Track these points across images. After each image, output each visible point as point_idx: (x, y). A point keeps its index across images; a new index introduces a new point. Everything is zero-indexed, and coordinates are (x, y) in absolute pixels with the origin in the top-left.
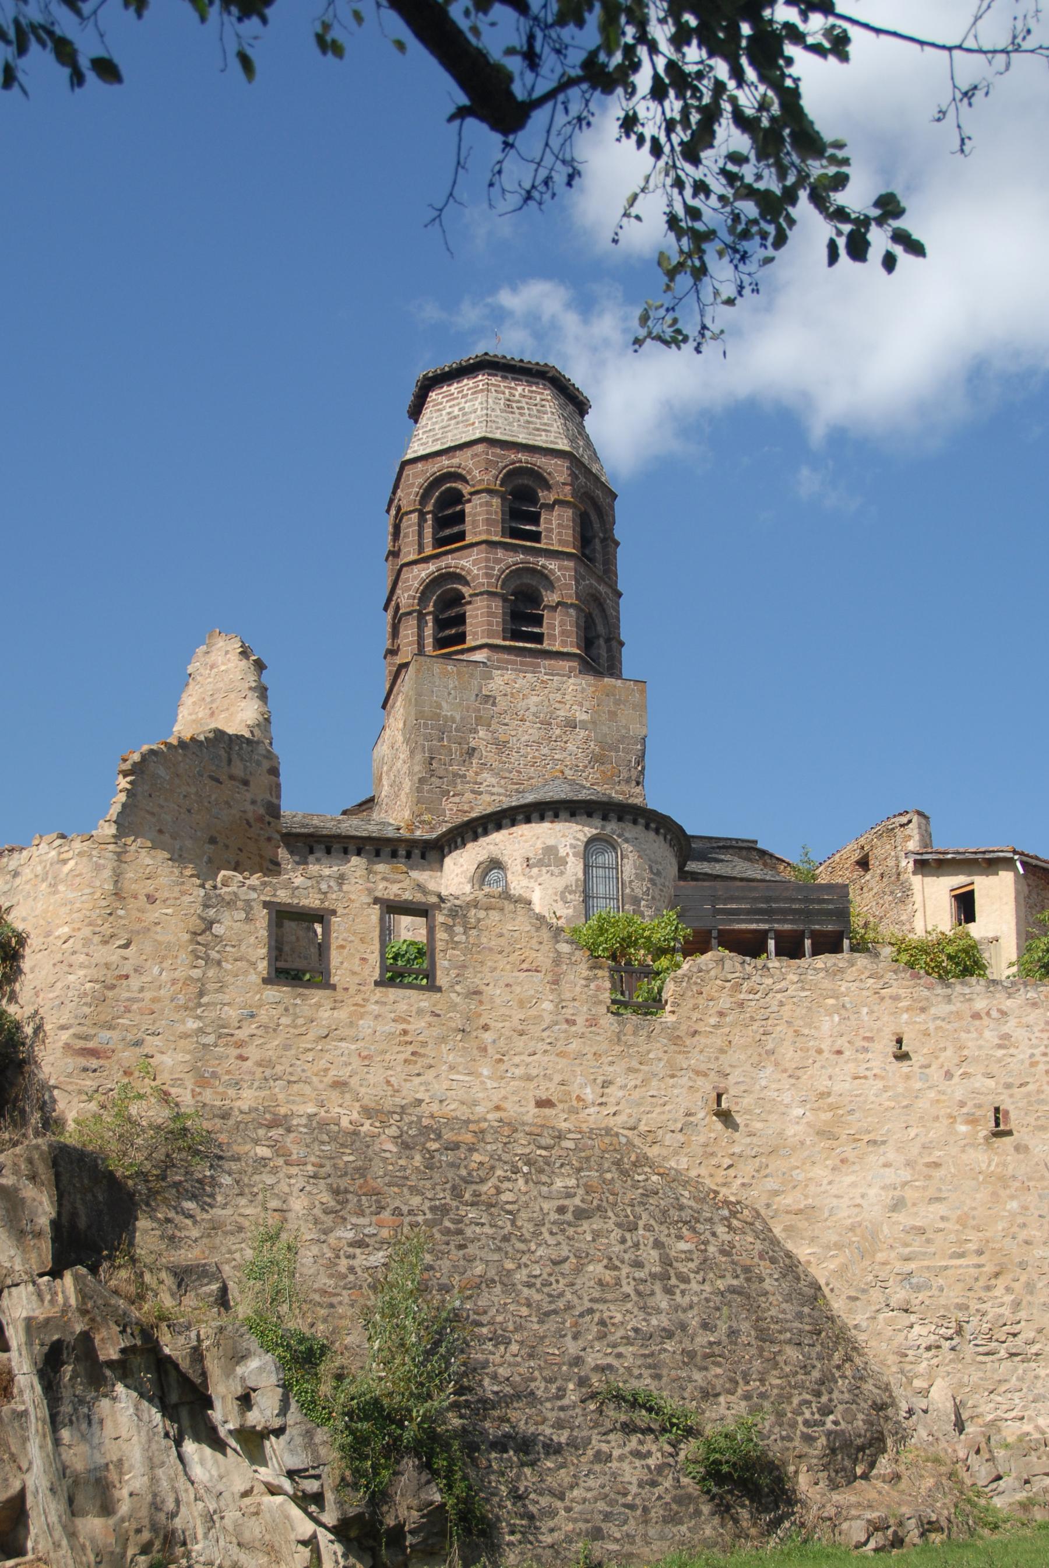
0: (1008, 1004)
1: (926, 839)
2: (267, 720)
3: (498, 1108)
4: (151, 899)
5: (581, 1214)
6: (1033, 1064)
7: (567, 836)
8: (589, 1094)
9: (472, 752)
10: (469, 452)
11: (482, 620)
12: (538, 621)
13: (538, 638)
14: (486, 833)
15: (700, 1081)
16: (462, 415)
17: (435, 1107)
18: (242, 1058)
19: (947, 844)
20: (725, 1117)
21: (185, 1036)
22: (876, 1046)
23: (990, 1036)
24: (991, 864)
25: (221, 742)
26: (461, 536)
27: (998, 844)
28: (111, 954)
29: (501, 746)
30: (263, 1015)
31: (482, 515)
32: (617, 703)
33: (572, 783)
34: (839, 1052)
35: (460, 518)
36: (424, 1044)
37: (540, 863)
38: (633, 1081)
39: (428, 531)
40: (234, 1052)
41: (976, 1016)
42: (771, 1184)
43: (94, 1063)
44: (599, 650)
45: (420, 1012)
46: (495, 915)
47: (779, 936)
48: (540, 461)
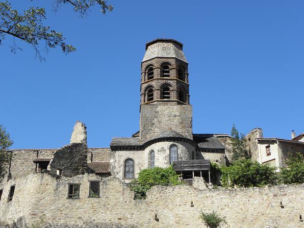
0: (213, 194)
1: (261, 135)
2: (86, 139)
3: (110, 220)
4: (47, 184)
6: (218, 207)
7: (166, 145)
8: (129, 216)
10: (154, 60)
11: (156, 95)
13: (169, 98)
14: (151, 144)
15: (152, 213)
16: (155, 52)
17: (98, 221)
18: (62, 214)
19: (266, 137)
20: (157, 220)
21: (52, 210)
22: (188, 204)
23: (210, 202)
24: (273, 142)
25: (76, 145)
26: (153, 77)
27: (274, 137)
28: (39, 195)
29: (160, 122)
30: (66, 205)
31: (157, 73)
32: (185, 110)
33: (173, 131)
34: (180, 205)
35: (153, 73)
36: (97, 209)
38: (138, 213)
39: (146, 76)
40: (60, 212)
41: (207, 197)
43: (34, 216)
44: (183, 97)
46: (112, 182)
47: (195, 171)
48: (169, 60)
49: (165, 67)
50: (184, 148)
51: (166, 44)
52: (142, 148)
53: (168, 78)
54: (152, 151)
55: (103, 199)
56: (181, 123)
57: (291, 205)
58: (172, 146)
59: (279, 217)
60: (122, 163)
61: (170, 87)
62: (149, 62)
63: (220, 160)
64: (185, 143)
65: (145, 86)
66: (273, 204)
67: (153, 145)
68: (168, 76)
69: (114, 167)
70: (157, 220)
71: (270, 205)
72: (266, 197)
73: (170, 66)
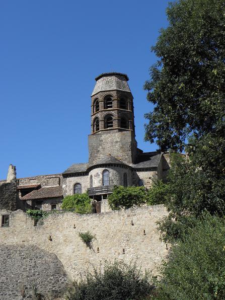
5: (24, 258)
7: (99, 170)
9: (98, 151)
11: (101, 124)
12: (112, 123)
13: (112, 126)
16: (102, 86)
17: (8, 244)
20: (51, 240)
23: (86, 224)
29: (104, 149)
37: (96, 176)
42: (57, 250)
45: (7, 230)
47: (103, 195)
49: (108, 99)
50: (115, 172)
51: (109, 78)
52: (86, 173)
54: (91, 176)
55: (11, 228)
56: (122, 148)
57: (138, 222)
58: (104, 171)
59: (130, 232)
60: (72, 187)
61: (113, 117)
62: (96, 96)
63: (152, 177)
64: (116, 167)
65: (94, 117)
66: (127, 223)
68: (111, 107)
69: (66, 191)
70: (51, 240)
71: (125, 224)
72: (122, 218)
73: (112, 98)
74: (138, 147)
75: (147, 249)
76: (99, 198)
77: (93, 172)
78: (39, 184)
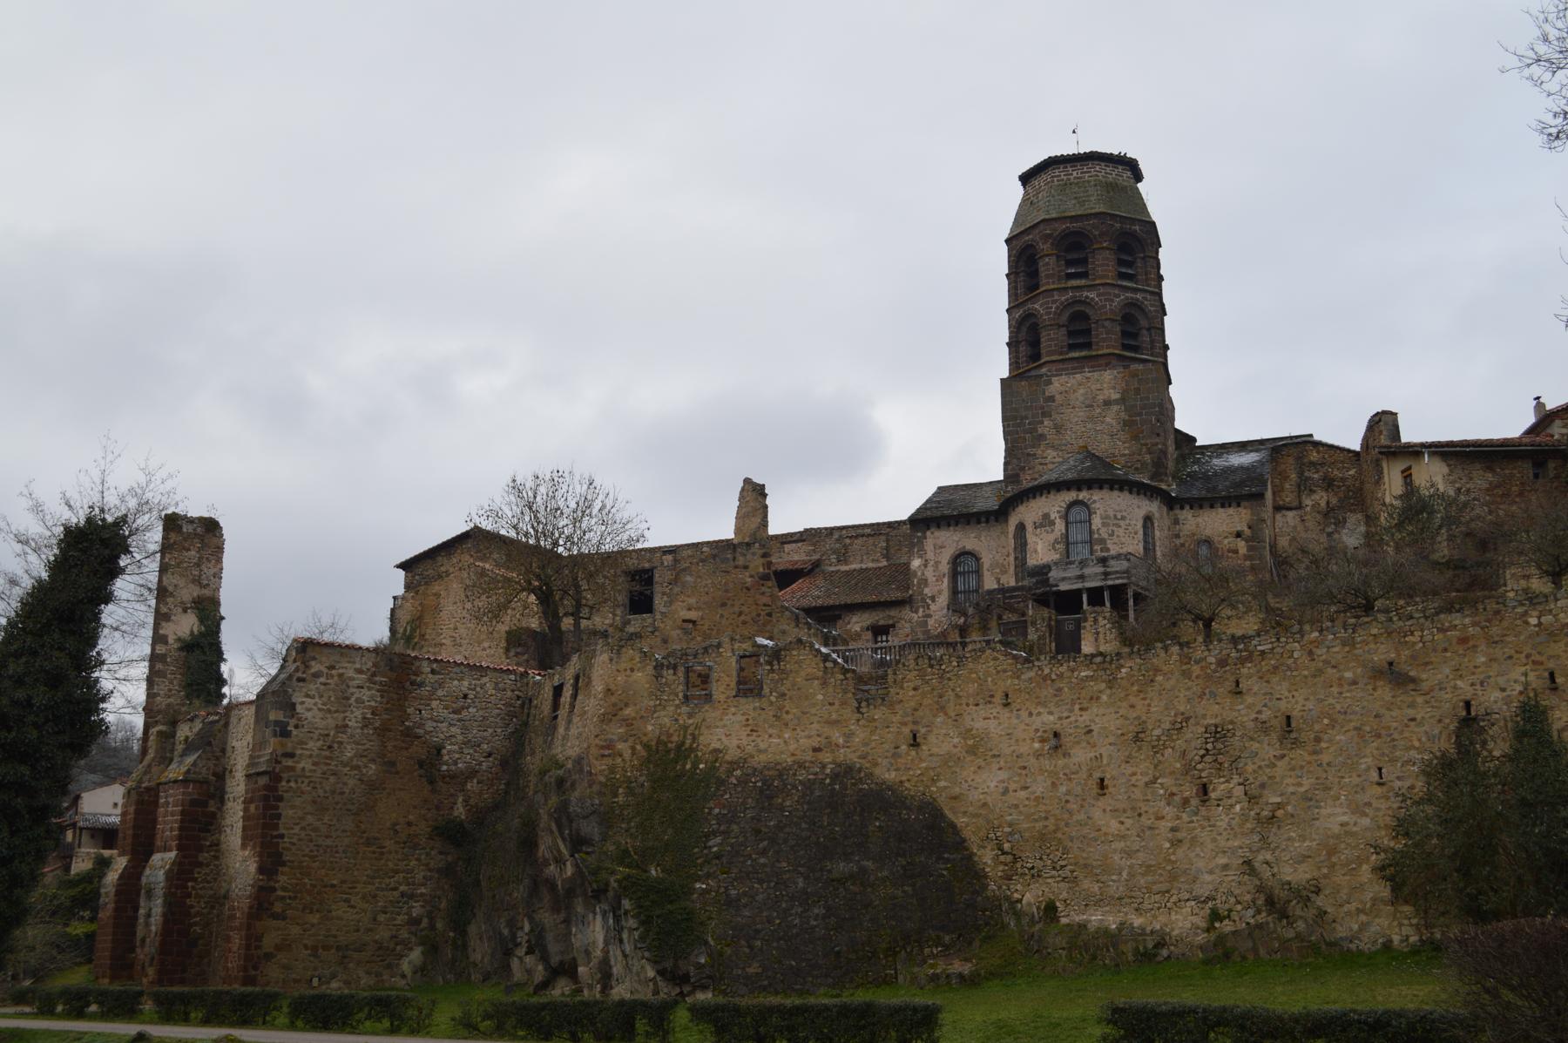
4: (632, 670)
37: (1042, 526)
47: (1089, 590)
53: (1083, 282)
54: (1021, 527)
60: (945, 567)
67: (1021, 509)
69: (925, 582)
74: (1179, 425)
75: (1300, 785)
76: (1068, 603)
77: (1029, 513)
78: (815, 557)
